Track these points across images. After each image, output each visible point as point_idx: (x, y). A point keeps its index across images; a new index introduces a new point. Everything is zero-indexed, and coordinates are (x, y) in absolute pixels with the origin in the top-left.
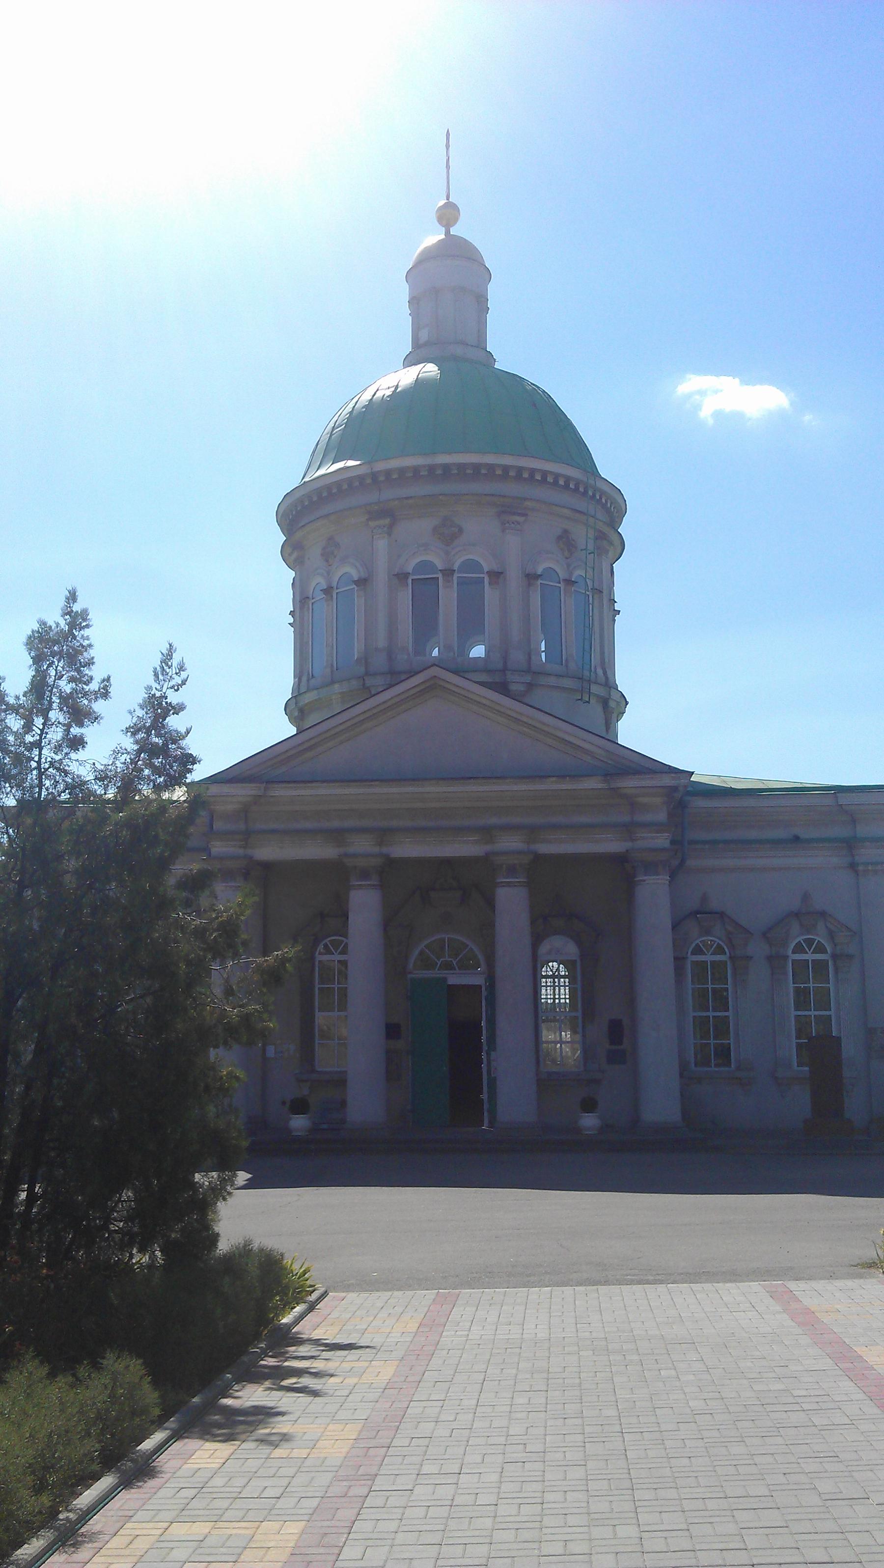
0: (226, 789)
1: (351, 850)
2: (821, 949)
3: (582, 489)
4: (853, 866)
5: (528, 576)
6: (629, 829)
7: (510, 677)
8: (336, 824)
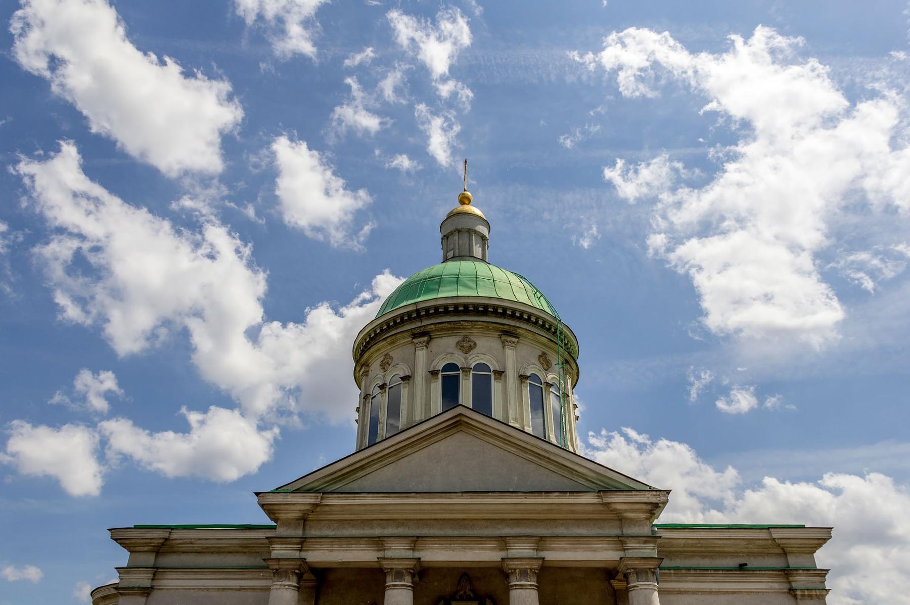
0: (291, 499)
1: (389, 554)
3: (553, 330)
4: (792, 591)
5: (521, 376)
6: (621, 541)
8: (377, 532)
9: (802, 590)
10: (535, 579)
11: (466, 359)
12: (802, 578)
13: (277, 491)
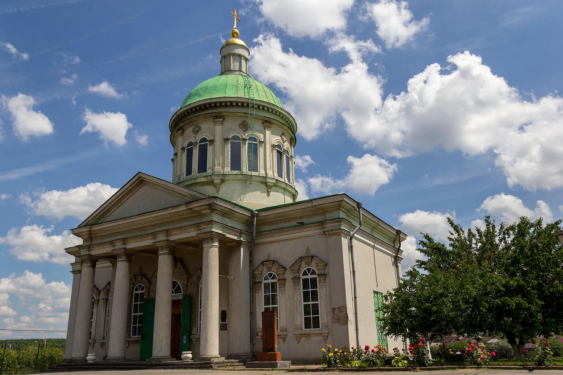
2: (313, 273)
7: (213, 177)
9: (328, 231)
10: (167, 250)
11: (195, 138)
12: (329, 225)
13: (79, 227)
